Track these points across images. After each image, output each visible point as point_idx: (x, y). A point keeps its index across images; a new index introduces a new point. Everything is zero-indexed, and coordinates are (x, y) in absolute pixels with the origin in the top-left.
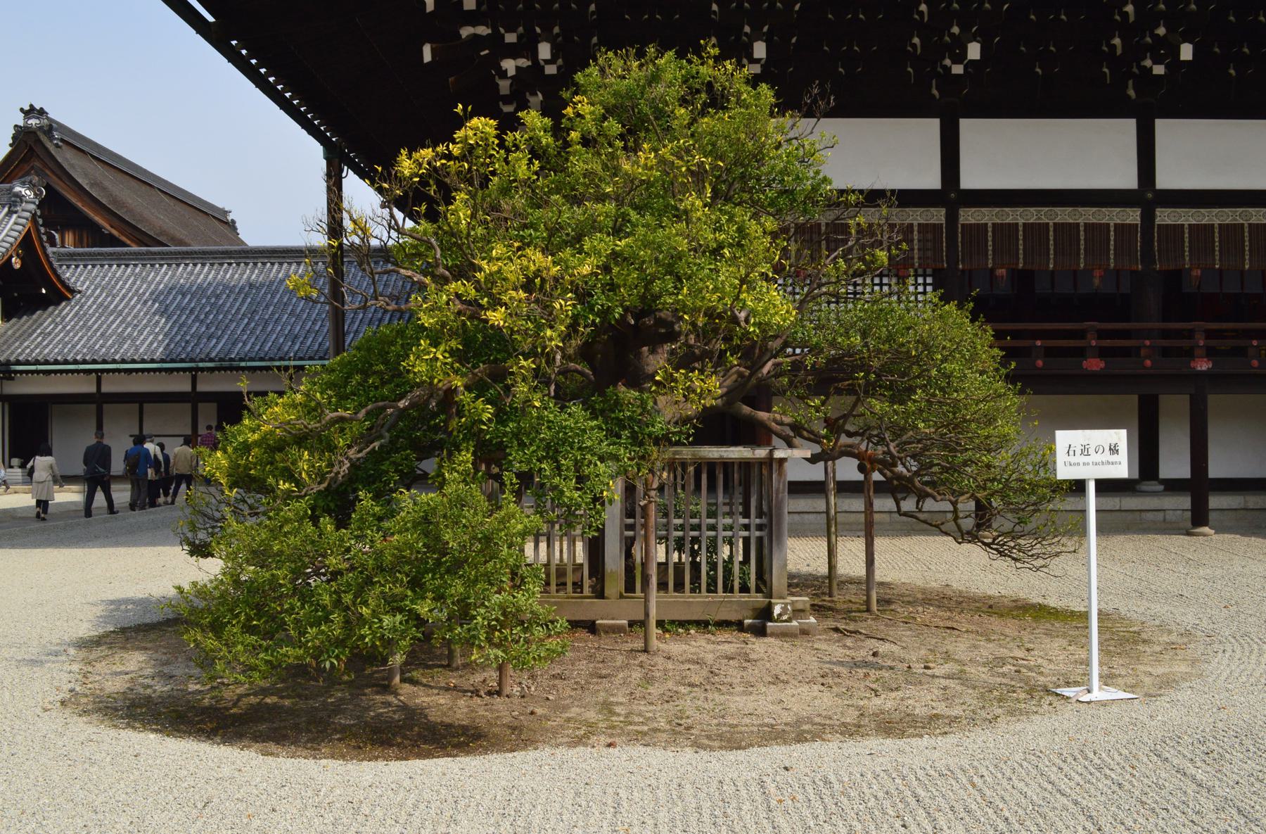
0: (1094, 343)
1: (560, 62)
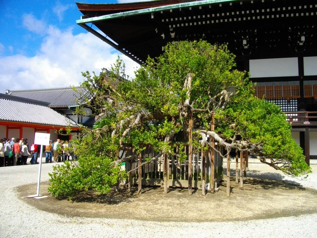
0: (307, 117)
1: (248, 45)
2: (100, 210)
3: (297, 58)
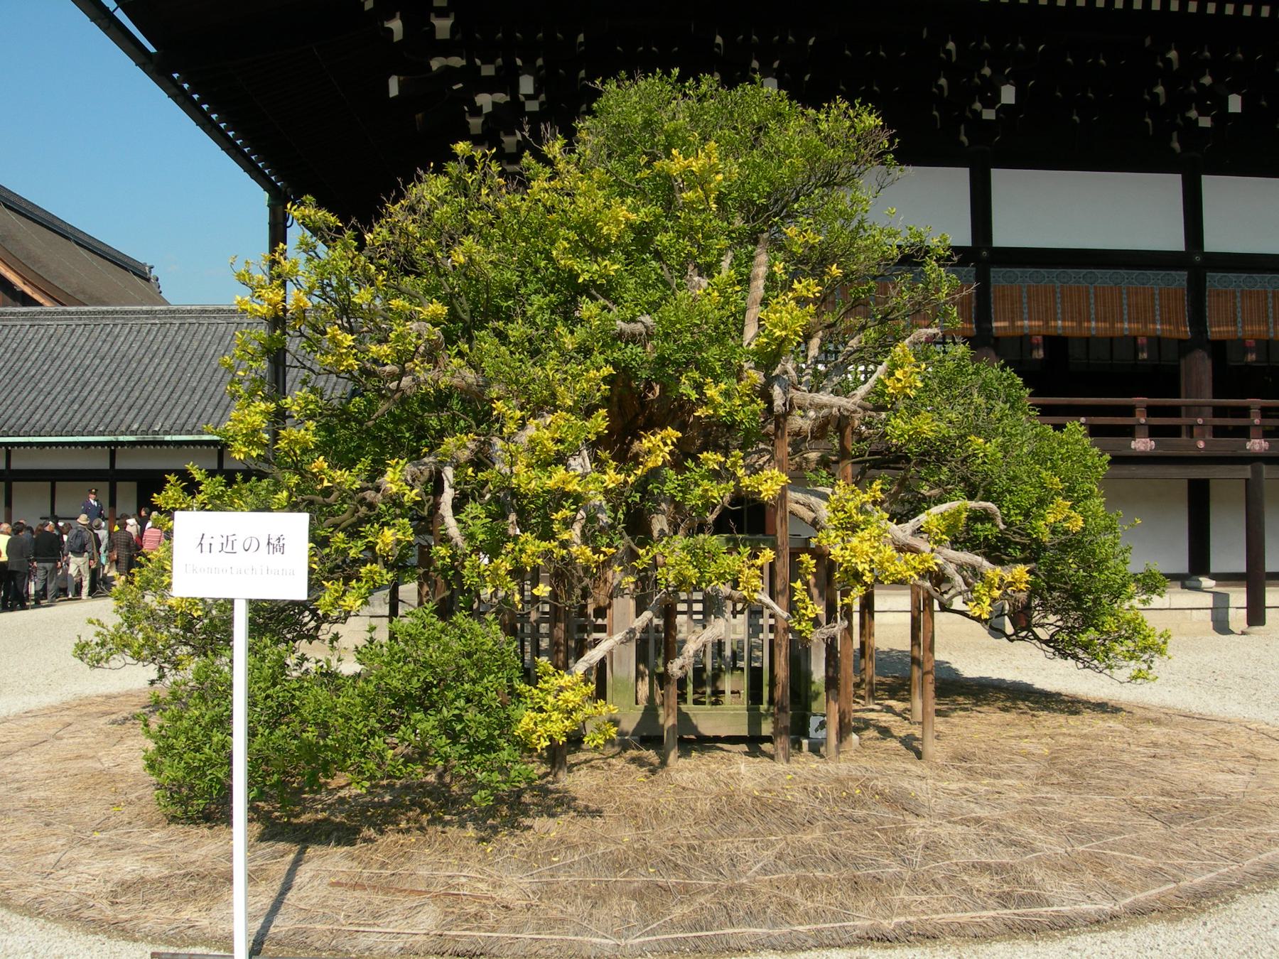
0: (1143, 421)
1: (543, 97)
2: (686, 910)
3: (1203, 177)
